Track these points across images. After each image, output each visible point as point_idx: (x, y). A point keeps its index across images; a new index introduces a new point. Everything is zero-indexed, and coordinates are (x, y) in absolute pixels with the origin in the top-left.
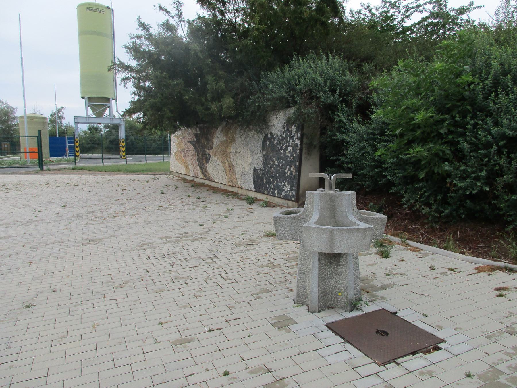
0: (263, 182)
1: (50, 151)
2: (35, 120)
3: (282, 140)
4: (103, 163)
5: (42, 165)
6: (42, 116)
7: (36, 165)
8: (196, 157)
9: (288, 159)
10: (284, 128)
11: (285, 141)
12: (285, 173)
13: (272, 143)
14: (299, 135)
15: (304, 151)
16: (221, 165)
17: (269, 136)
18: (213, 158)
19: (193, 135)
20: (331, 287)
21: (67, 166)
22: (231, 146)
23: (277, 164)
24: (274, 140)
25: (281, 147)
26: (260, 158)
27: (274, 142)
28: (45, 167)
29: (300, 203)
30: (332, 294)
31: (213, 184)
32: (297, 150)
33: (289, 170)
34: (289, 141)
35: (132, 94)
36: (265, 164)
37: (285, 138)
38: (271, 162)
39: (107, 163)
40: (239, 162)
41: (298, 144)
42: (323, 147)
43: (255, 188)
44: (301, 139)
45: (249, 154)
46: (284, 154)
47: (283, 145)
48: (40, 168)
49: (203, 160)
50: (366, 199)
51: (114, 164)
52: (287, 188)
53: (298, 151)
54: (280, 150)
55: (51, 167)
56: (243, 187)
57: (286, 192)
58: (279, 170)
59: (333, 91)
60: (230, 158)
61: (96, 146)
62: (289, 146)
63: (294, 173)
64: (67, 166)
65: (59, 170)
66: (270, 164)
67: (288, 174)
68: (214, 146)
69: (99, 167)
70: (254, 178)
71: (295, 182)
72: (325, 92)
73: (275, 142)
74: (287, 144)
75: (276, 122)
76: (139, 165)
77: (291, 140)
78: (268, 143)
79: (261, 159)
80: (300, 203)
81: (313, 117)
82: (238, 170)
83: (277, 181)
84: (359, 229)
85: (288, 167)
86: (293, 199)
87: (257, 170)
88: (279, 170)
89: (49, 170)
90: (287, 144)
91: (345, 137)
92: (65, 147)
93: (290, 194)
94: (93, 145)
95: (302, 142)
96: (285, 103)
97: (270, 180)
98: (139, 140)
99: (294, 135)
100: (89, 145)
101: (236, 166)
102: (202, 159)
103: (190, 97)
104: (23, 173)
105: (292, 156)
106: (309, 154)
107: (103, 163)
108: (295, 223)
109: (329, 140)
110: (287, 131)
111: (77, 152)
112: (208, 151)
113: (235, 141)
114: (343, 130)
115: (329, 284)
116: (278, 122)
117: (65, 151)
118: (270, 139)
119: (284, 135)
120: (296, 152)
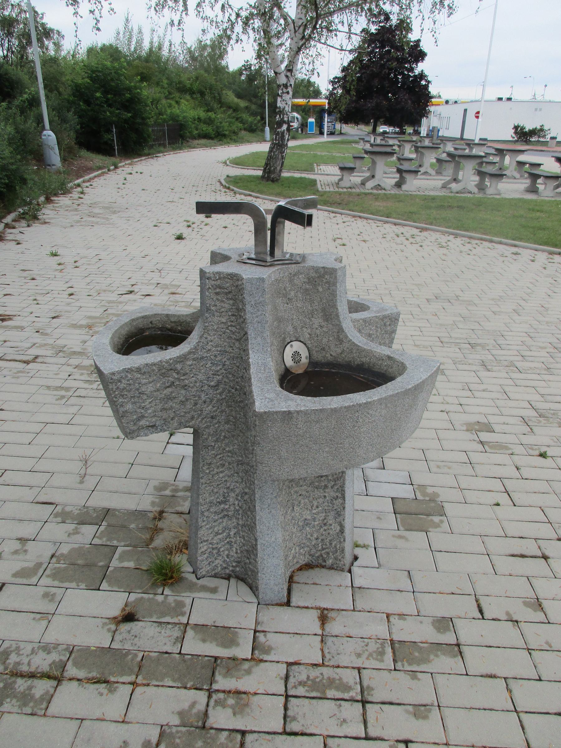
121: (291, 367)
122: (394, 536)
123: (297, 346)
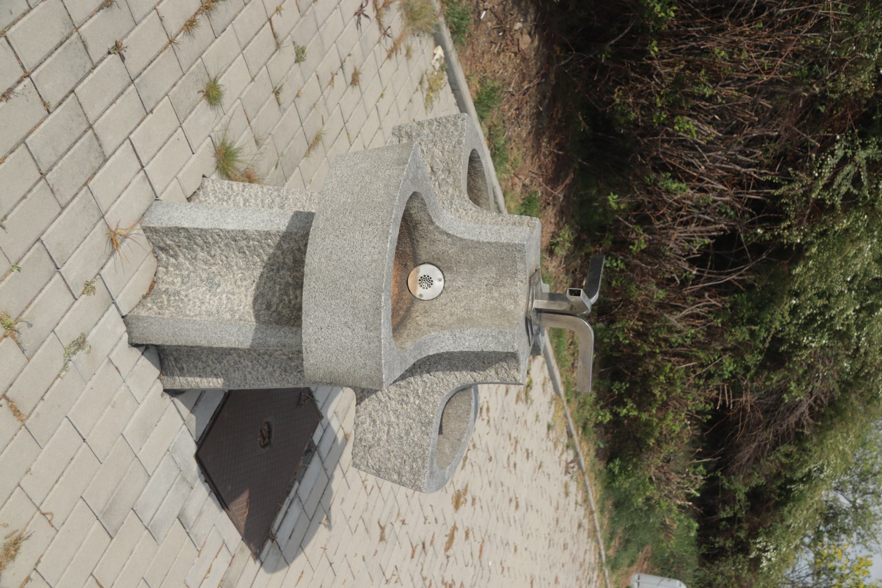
121: (418, 272)
123: (438, 285)
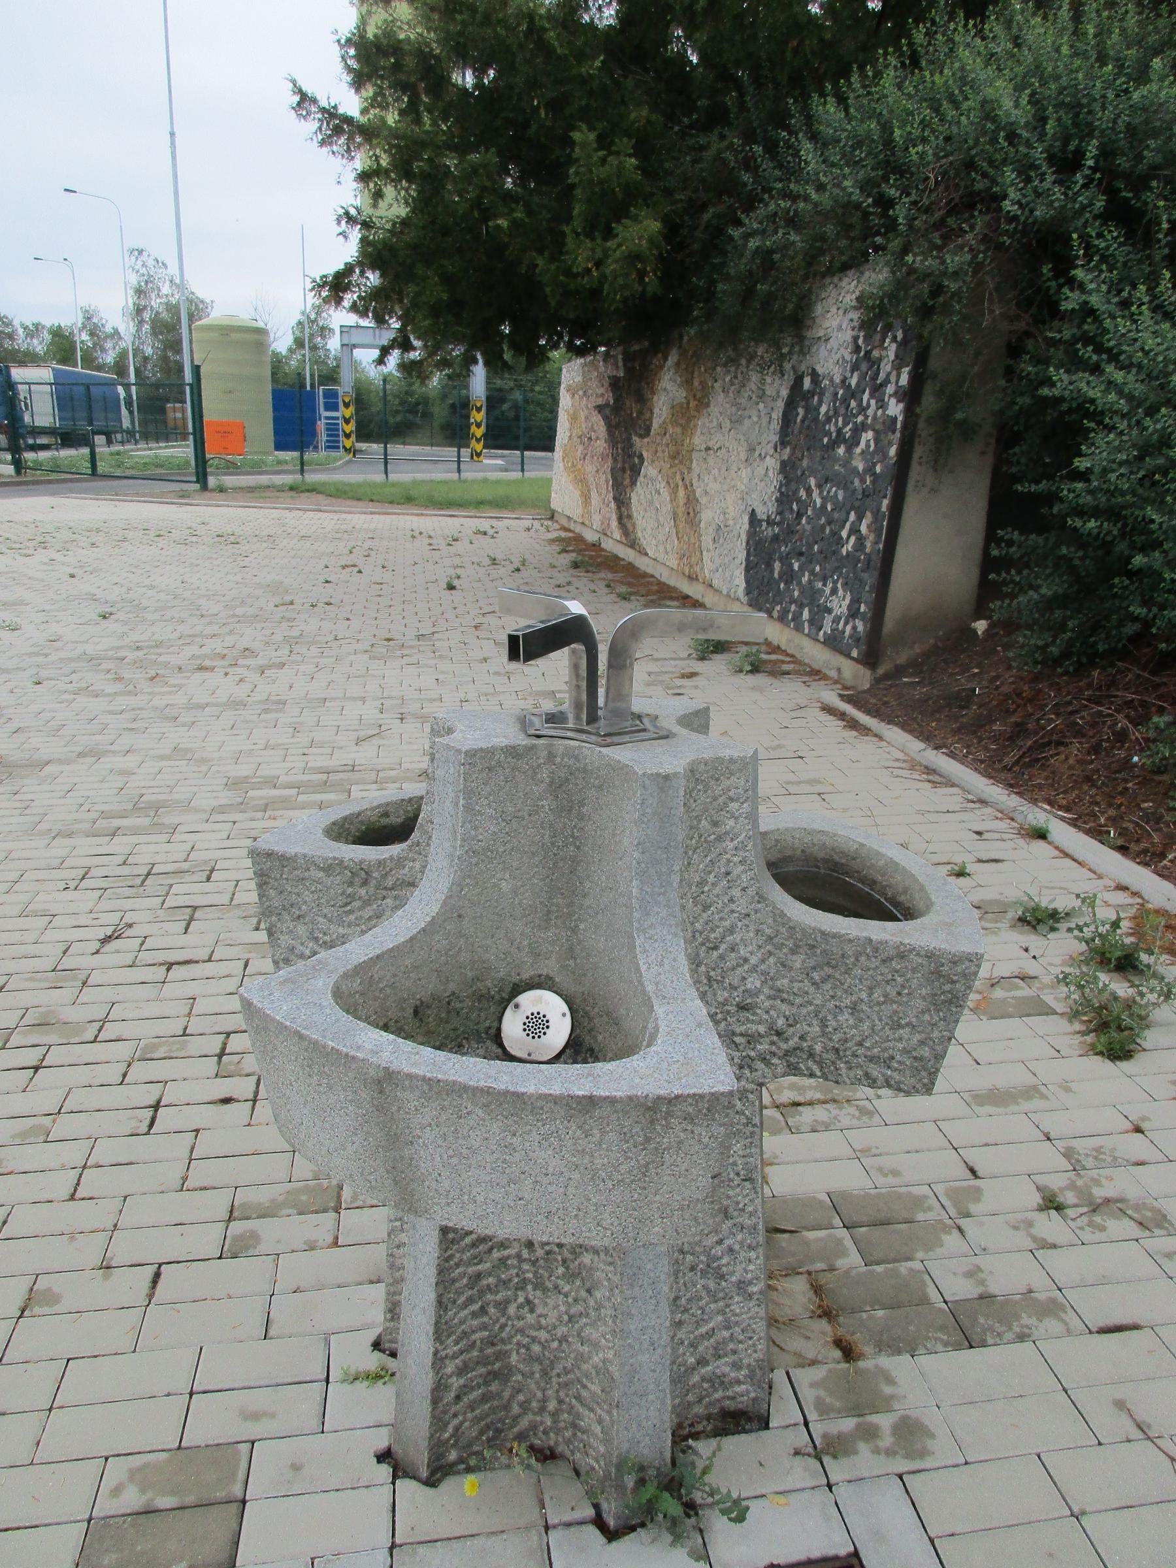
0: (772, 572)
1: (276, 433)
2: (235, 336)
3: (845, 402)
4: (459, 471)
5: (205, 475)
6: (254, 324)
7: (190, 474)
8: (610, 463)
9: (857, 482)
10: (857, 349)
11: (853, 404)
12: (840, 542)
13: (812, 411)
14: (904, 380)
15: (919, 451)
16: (665, 494)
17: (807, 383)
18: (649, 470)
19: (606, 383)
20: (543, 1335)
21: (279, 479)
22: (695, 426)
23: (819, 502)
24: (820, 402)
25: (839, 432)
26: (771, 473)
27: (817, 409)
28: (212, 481)
29: (881, 671)
30: (545, 1373)
31: (643, 564)
32: (890, 444)
33: (855, 530)
34: (869, 405)
35: (339, 222)
36: (784, 499)
37: (854, 394)
38: (802, 493)
39: (402, 476)
40: (713, 487)
41: (894, 420)
42: (1007, 436)
43: (748, 592)
44: (911, 397)
45: (743, 456)
46: (846, 463)
47: (845, 424)
48: (198, 481)
49: (625, 471)
50: (1157, 686)
51: (419, 476)
52: (840, 604)
53: (893, 451)
54: (834, 444)
55: (229, 481)
56: (715, 583)
57: (837, 620)
58: (823, 528)
59: (1066, 164)
60: (690, 469)
61: (418, 420)
62: (864, 427)
63: (868, 544)
64: (279, 479)
65: (251, 489)
66: (799, 501)
67: (849, 546)
68: (655, 425)
69: (373, 485)
70: (748, 554)
71: (870, 579)
72: (1026, 170)
73: (823, 409)
74: (860, 419)
75: (835, 324)
76: (497, 482)
77: (873, 402)
78: (801, 411)
79: (775, 480)
80: (881, 671)
81: (957, 295)
82: (708, 516)
83: (812, 573)
84: (591, 1101)
85: (852, 516)
86: (855, 653)
87: (760, 521)
88: (823, 528)
89: (221, 490)
90: (860, 419)
91: (1089, 387)
92: (313, 422)
93: (848, 628)
94: (410, 417)
95: (909, 412)
96: (857, 234)
97: (791, 565)
98: (539, 404)
99: (887, 381)
100: (399, 418)
101: (703, 500)
102: (623, 470)
103: (515, 224)
104: (162, 494)
105: (870, 470)
106: (938, 462)
107: (459, 471)
108: (367, 903)
109: (1025, 401)
110: (865, 361)
111: (348, 436)
112: (635, 439)
113: (708, 405)
114: (1087, 352)
115: (530, 1318)
116: (836, 324)
117: (314, 434)
118: (807, 396)
119: (854, 382)
120: (885, 456)
122: (273, 1416)
